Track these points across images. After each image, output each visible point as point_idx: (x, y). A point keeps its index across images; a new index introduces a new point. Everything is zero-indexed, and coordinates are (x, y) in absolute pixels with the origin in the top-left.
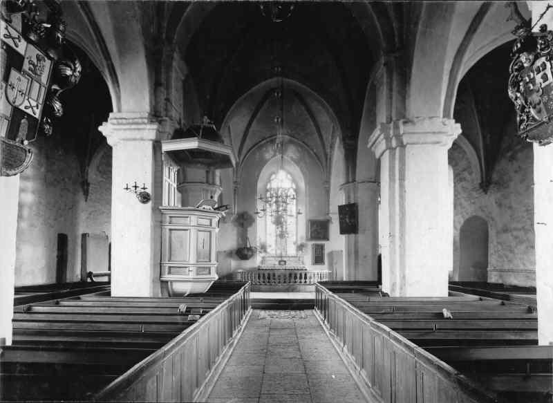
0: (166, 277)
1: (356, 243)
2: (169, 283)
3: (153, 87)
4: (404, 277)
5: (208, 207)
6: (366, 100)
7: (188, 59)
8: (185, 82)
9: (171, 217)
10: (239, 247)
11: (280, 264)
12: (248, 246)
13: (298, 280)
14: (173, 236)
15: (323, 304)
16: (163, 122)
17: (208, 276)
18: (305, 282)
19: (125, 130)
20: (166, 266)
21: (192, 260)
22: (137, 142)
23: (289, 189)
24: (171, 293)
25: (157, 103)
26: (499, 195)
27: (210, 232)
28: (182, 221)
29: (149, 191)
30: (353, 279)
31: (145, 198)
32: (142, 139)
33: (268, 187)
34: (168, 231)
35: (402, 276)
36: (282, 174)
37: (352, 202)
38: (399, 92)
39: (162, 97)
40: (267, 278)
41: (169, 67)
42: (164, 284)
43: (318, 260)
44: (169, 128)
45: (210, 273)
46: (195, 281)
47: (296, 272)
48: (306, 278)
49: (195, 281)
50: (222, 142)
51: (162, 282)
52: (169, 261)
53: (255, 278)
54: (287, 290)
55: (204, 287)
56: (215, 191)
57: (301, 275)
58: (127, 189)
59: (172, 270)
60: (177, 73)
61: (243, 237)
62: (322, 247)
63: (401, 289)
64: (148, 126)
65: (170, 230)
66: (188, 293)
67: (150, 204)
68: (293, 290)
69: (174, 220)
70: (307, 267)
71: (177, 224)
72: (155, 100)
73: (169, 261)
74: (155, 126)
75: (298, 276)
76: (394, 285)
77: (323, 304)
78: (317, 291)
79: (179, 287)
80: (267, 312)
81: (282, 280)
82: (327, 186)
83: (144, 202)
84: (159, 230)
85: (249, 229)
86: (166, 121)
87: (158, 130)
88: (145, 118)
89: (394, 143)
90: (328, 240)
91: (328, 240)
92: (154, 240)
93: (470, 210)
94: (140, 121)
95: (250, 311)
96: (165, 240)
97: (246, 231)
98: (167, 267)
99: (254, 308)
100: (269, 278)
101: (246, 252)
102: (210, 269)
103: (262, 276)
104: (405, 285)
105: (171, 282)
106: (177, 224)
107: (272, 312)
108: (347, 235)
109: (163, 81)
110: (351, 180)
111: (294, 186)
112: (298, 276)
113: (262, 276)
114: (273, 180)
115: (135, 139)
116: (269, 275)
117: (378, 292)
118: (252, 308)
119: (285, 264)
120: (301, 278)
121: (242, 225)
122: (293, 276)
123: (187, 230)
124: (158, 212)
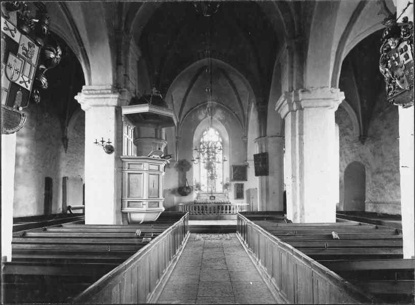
0: (126, 209)
1: (267, 183)
3: (115, 66)
11: (210, 199)
12: (187, 186)
13: (224, 211)
18: (230, 212)
20: (126, 200)
24: (129, 221)
26: (373, 145)
27: (159, 175)
28: (138, 167)
29: (113, 144)
30: (265, 210)
31: (110, 150)
32: (107, 105)
33: (202, 140)
36: (212, 131)
37: (264, 152)
40: (201, 210)
42: (125, 215)
44: (127, 97)
48: (230, 209)
49: (147, 212)
50: (167, 107)
52: (129, 169)
54: (216, 219)
55: (154, 217)
56: (162, 144)
58: (96, 143)
59: (131, 204)
60: (133, 54)
61: (183, 178)
62: (242, 186)
64: (112, 96)
65: (129, 174)
66: (141, 222)
67: (113, 154)
69: (131, 166)
74: (117, 96)
82: (246, 140)
83: (109, 153)
85: (187, 173)
90: (246, 180)
91: (246, 180)
93: (352, 157)
94: (105, 91)
95: (188, 234)
97: (185, 173)
99: (191, 232)
100: (202, 210)
101: (185, 191)
102: (158, 203)
104: (304, 214)
105: (130, 213)
107: (205, 235)
109: (123, 62)
110: (263, 135)
111: (221, 141)
114: (205, 135)
116: (202, 206)
119: (215, 199)
120: (226, 209)
124: (119, 160)
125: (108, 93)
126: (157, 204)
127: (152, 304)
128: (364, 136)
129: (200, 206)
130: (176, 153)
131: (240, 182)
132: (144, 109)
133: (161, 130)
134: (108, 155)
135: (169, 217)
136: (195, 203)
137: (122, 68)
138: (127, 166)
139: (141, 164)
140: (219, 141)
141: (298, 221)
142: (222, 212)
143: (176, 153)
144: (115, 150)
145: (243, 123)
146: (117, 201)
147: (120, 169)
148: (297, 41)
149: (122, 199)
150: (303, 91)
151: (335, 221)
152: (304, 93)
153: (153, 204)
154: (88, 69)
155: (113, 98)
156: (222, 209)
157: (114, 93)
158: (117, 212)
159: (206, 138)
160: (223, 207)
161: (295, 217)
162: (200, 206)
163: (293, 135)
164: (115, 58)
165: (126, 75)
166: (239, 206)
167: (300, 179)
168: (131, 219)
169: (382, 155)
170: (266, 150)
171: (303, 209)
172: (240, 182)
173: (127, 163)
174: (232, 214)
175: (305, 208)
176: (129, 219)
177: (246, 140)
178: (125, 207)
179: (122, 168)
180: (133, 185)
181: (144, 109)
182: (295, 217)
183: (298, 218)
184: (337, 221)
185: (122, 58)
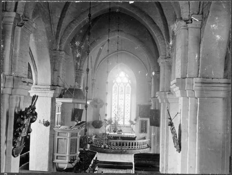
2: (57, 164)
4: (167, 165)
6: (195, 1)
10: (94, 120)
14: (59, 141)
15: (144, 143)
19: (39, 92)
20: (56, 154)
22: (44, 98)
29: (49, 121)
31: (47, 124)
32: (47, 97)
35: (166, 165)
37: (157, 109)
39: (56, 77)
42: (54, 164)
51: (53, 163)
52: (58, 136)
59: (58, 157)
64: (50, 92)
65: (58, 139)
66: (65, 168)
67: (49, 127)
73: (58, 136)
74: (53, 92)
76: (163, 168)
77: (144, 143)
87: (54, 93)
88: (49, 88)
94: (46, 89)
96: (55, 147)
98: (57, 139)
104: (167, 169)
105: (58, 163)
110: (200, 12)
115: (43, 97)
123: (66, 133)
127: (1, 170)
133: (79, 105)
134: (45, 127)
139: (66, 133)
144: (50, 124)
145: (148, 70)
147: (53, 135)
149: (53, 154)
150: (169, 94)
152: (170, 95)
154: (36, 72)
155: (50, 93)
157: (52, 89)
158: (49, 162)
159: (118, 80)
161: (162, 171)
167: (166, 147)
170: (158, 108)
174: (134, 149)
176: (57, 166)
178: (54, 160)
179: (54, 135)
182: (162, 171)
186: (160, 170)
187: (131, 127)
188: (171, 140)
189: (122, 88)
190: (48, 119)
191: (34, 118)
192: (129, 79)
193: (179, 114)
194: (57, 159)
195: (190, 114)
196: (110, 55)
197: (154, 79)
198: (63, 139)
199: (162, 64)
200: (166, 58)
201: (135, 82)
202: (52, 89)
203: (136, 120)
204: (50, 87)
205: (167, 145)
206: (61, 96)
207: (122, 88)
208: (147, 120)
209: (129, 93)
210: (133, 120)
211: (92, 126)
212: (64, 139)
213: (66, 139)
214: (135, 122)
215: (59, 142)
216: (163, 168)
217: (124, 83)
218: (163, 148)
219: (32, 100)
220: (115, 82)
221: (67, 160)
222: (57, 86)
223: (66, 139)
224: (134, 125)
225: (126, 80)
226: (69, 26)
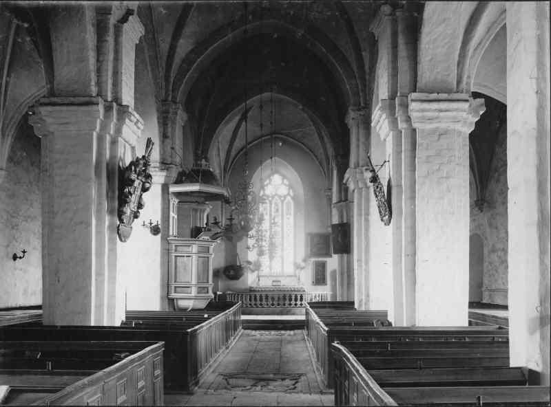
0: (173, 295)
3: (162, 138)
5: (206, 238)
7: (188, 108)
8: (184, 127)
9: (176, 246)
10: (228, 264)
13: (293, 302)
14: (178, 260)
16: (169, 169)
17: (207, 295)
18: (301, 304)
21: (194, 282)
23: (285, 197)
24: (176, 308)
25: (164, 152)
26: (489, 214)
27: (208, 258)
28: (186, 249)
30: (345, 300)
31: (155, 230)
34: (173, 257)
36: (277, 178)
37: (345, 221)
38: (364, 143)
39: (168, 149)
40: (256, 299)
41: (174, 123)
42: (171, 301)
43: (320, 279)
44: (174, 175)
45: (208, 292)
46: (196, 298)
47: (285, 293)
48: (301, 300)
49: (196, 298)
50: (218, 185)
51: (169, 299)
53: (246, 299)
54: (281, 313)
55: (202, 304)
56: (206, 209)
57: (296, 296)
58: (144, 225)
60: (181, 117)
61: (232, 253)
63: (366, 304)
64: (159, 173)
65: (176, 256)
67: (159, 236)
68: (287, 314)
69: (179, 248)
70: (305, 288)
71: (182, 252)
72: (163, 149)
74: (164, 173)
75: (293, 297)
76: (361, 301)
78: (307, 314)
79: (182, 304)
80: (258, 332)
81: (270, 302)
82: (329, 194)
83: (155, 234)
84: (166, 257)
86: (172, 167)
87: (166, 176)
88: (156, 162)
89: (361, 185)
92: (162, 264)
95: (241, 331)
97: (235, 247)
99: (245, 328)
100: (261, 300)
102: (207, 288)
103: (253, 297)
104: (369, 301)
106: (182, 252)
107: (263, 332)
108: (340, 255)
109: (169, 134)
110: (343, 199)
111: (292, 194)
112: (293, 297)
113: (253, 297)
114: (267, 185)
116: (261, 296)
117: (353, 308)
118: (243, 328)
120: (296, 300)
121: (229, 239)
122: (287, 298)
124: (165, 240)
125: (155, 171)
126: (206, 289)
128: (482, 200)
129: (264, 294)
130: (222, 214)
131: (321, 259)
132: (195, 187)
135: (218, 305)
136: (251, 291)
137: (168, 141)
138: (174, 247)
140: (289, 194)
141: (363, 309)
142: (290, 304)
143: (222, 214)
144: (161, 231)
146: (162, 286)
148: (362, 113)
151: (466, 324)
153: (202, 290)
156: (290, 300)
158: (162, 298)
159: (269, 190)
160: (290, 296)
161: (360, 305)
162: (264, 294)
163: (360, 215)
164: (162, 129)
165: (173, 148)
166: (319, 296)
168: (178, 306)
169: (497, 228)
171: (368, 296)
172: (321, 259)
173: (174, 245)
175: (371, 293)
177: (329, 194)
179: (168, 250)
180: (180, 269)
181: (195, 187)
182: (360, 305)
183: (363, 306)
184: (470, 324)
185: (170, 130)
186: (356, 306)
187: (295, 276)
188: (374, 203)
189: (276, 204)
190: (157, 218)
191: (148, 182)
192: (291, 187)
193: (387, 164)
194: (175, 292)
195: (405, 236)
196: (250, 143)
197: (338, 170)
198: (184, 256)
199: (353, 121)
200: (359, 110)
201: (301, 191)
202: (162, 169)
203: (305, 261)
204: (158, 165)
205: (367, 214)
206: (178, 181)
207: (276, 204)
208: (326, 262)
209: (290, 214)
210: (299, 261)
211: (224, 276)
212: (187, 256)
213: (189, 256)
214: (303, 264)
215: (178, 263)
216: (361, 301)
217: (280, 197)
218: (360, 266)
219: (147, 146)
220: (264, 195)
221: (194, 292)
222: (170, 164)
223: (189, 256)
224: (303, 271)
225: (283, 190)
226: (188, 61)
